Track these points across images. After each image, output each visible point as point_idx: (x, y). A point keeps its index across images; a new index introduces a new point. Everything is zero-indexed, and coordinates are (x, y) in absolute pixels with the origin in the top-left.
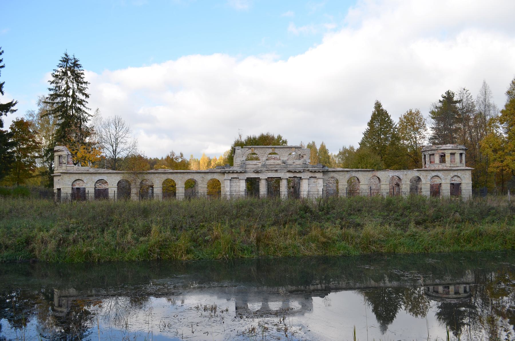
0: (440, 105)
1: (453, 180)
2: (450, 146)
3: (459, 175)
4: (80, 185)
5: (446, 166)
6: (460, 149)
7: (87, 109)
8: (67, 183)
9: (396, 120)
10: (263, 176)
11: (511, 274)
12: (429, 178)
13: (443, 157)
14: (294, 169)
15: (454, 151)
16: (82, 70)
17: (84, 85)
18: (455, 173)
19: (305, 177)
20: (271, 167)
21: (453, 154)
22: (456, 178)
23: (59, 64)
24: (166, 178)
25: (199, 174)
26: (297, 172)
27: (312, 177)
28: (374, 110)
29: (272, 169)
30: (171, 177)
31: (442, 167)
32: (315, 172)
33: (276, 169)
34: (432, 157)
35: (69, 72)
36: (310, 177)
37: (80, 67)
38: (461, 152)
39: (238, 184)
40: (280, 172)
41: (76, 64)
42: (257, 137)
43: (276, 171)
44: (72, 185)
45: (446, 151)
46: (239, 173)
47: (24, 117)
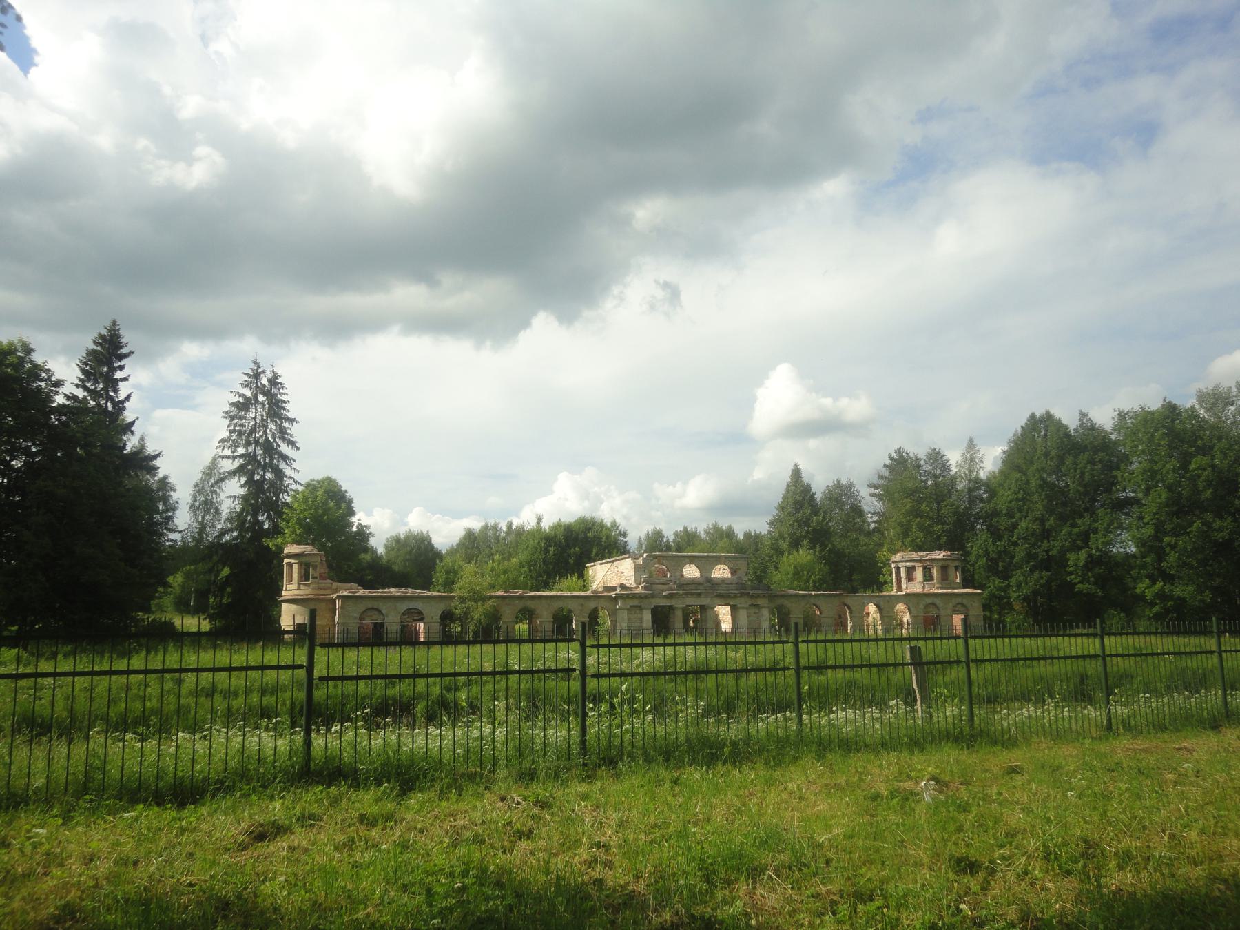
0: (886, 473)
3: (965, 601)
11: (790, 509)
15: (946, 563)
16: (284, 394)
17: (286, 425)
18: (959, 600)
19: (743, 605)
23: (245, 381)
35: (261, 398)
39: (639, 616)
41: (274, 382)
43: (699, 595)
44: (361, 618)
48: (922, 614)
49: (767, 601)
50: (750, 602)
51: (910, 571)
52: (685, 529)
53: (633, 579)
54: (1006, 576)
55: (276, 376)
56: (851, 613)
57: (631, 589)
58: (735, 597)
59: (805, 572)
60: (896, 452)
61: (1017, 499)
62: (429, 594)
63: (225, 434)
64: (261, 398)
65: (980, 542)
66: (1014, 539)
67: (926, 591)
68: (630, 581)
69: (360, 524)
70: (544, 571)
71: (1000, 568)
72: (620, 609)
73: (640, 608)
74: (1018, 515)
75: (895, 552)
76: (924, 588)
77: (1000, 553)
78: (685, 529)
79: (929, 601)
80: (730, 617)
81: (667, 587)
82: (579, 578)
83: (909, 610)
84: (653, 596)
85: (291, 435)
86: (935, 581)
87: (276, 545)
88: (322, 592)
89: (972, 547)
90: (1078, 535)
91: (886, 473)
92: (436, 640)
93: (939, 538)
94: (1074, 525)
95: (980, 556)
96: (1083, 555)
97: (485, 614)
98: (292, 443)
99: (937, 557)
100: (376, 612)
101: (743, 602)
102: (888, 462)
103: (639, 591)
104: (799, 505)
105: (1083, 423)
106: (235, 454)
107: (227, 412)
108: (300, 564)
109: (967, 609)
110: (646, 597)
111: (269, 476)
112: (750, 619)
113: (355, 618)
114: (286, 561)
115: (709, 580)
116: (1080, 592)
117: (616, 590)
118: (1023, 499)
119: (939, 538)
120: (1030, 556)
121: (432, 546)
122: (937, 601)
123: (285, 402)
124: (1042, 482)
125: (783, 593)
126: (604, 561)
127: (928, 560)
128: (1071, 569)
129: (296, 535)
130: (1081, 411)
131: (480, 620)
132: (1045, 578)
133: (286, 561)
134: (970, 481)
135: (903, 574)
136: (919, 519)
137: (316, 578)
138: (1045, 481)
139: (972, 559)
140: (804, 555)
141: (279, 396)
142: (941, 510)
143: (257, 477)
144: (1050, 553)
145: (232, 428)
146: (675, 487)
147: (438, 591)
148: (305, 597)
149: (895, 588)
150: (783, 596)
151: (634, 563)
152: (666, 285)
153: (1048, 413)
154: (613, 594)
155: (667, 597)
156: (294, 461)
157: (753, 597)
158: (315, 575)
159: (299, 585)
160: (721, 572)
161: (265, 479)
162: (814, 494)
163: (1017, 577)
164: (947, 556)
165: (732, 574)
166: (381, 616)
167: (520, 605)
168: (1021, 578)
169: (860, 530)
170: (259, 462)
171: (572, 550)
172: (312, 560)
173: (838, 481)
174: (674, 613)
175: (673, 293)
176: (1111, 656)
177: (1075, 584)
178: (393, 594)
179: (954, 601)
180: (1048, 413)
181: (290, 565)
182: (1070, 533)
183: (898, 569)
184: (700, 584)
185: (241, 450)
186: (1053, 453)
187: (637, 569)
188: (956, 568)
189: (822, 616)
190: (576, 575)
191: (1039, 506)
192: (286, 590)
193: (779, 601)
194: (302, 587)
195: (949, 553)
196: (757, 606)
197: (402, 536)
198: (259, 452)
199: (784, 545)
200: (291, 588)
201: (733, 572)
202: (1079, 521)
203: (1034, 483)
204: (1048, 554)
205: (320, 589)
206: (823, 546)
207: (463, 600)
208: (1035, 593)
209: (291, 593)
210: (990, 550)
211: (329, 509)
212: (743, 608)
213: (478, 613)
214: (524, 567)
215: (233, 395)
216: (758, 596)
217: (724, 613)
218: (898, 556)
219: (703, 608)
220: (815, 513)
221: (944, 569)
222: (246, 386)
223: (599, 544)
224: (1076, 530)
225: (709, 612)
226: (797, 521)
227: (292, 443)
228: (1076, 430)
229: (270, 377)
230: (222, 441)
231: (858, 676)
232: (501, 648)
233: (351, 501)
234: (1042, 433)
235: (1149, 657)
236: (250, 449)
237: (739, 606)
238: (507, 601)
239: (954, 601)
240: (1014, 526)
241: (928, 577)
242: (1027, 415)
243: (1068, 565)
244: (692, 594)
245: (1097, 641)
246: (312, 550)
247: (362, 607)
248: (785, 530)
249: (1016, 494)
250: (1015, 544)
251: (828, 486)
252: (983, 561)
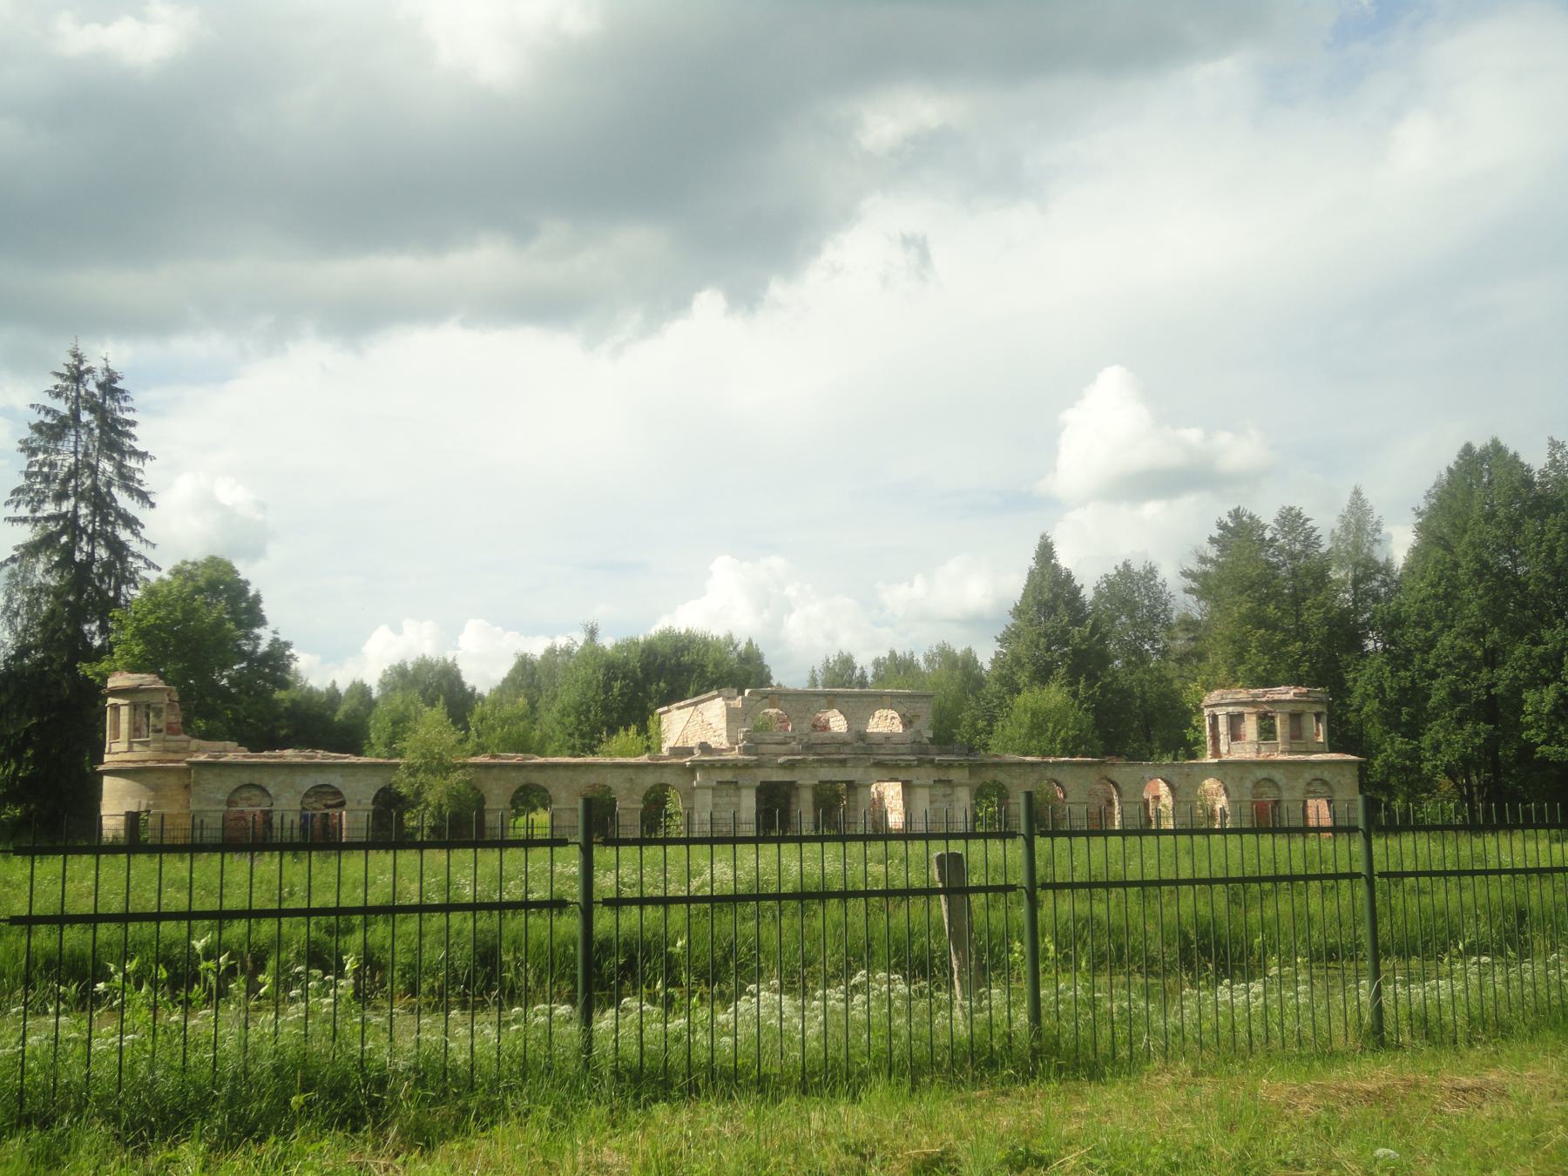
0: (1212, 552)
2: (1287, 693)
3: (1327, 776)
4: (254, 802)
7: (144, 545)
8: (212, 795)
10: (807, 779)
12: (1249, 784)
14: (893, 757)
15: (1300, 707)
16: (129, 409)
17: (131, 463)
18: (1317, 773)
20: (827, 749)
23: (56, 387)
25: (621, 770)
26: (903, 767)
27: (940, 781)
28: (1033, 564)
29: (831, 757)
33: (843, 756)
35: (86, 417)
36: (935, 781)
37: (125, 399)
38: (1319, 708)
39: (734, 799)
40: (853, 767)
41: (109, 387)
43: (843, 763)
46: (740, 768)
47: (271, 627)
48: (1250, 798)
49: (967, 772)
50: (935, 775)
51: (1235, 721)
52: (893, 654)
53: (725, 734)
54: (1413, 731)
55: (112, 377)
56: (1120, 795)
57: (720, 751)
58: (909, 766)
59: (1051, 725)
60: (1230, 516)
61: (1436, 596)
62: (363, 760)
63: (21, 481)
64: (86, 417)
65: (1368, 671)
66: (1430, 666)
67: (1261, 757)
68: (719, 739)
69: (276, 640)
70: (603, 723)
71: (1404, 718)
72: (700, 787)
74: (1437, 624)
75: (1209, 688)
76: (1258, 752)
77: (1403, 691)
78: (893, 654)
79: (1261, 774)
80: (901, 802)
81: (783, 748)
82: (639, 734)
83: (1226, 790)
84: (759, 765)
85: (140, 482)
86: (1279, 740)
87: (97, 674)
88: (171, 756)
89: (1355, 680)
90: (1544, 660)
91: (1212, 552)
92: (750, 835)
93: (1296, 665)
94: (1535, 642)
95: (1368, 695)
96: (1550, 694)
97: (450, 796)
98: (143, 497)
99: (1283, 697)
100: (257, 792)
101: (924, 776)
102: (1216, 533)
103: (735, 755)
104: (1048, 608)
105: (1555, 460)
106: (38, 514)
107: (25, 441)
108: (134, 707)
109: (1331, 789)
110: (746, 766)
111: (102, 553)
112: (936, 805)
113: (220, 802)
114: (111, 701)
115: (862, 737)
116: (1544, 761)
117: (693, 754)
118: (1446, 596)
119: (1296, 665)
120: (1456, 696)
121: (462, 684)
122: (1278, 775)
123: (133, 424)
124: (1477, 566)
125: (996, 759)
126: (682, 704)
127: (1267, 702)
128: (1530, 718)
129: (133, 656)
130: (1551, 439)
131: (440, 806)
132: (1483, 735)
133: (111, 701)
134: (1356, 565)
135: (1223, 728)
136: (1262, 631)
137: (160, 731)
138: (1485, 565)
139: (1355, 701)
140: (1054, 695)
141: (119, 414)
142: (1302, 615)
144: (1493, 692)
145: (36, 469)
146: (911, 585)
147: (378, 756)
148: (141, 765)
149: (1209, 752)
150: (996, 765)
151: (727, 705)
152: (907, 242)
153: (1495, 443)
154: (687, 761)
155: (783, 766)
156: (143, 527)
158: (159, 727)
159: (131, 743)
160: (884, 723)
161: (94, 560)
162: (1077, 591)
163: (1434, 732)
164: (1302, 695)
165: (905, 725)
166: (267, 799)
167: (519, 779)
168: (1440, 736)
170: (84, 530)
171: (654, 687)
172: (155, 699)
173: (1126, 565)
174: (798, 796)
175: (917, 246)
177: (1537, 745)
178: (288, 760)
179: (1308, 775)
180: (1495, 443)
181: (116, 708)
182: (1528, 655)
183: (1215, 718)
184: (845, 744)
185: (49, 508)
186: (1501, 513)
187: (732, 716)
188: (1318, 716)
189: (1067, 800)
190: (633, 729)
191: (1474, 607)
192: (109, 753)
193: (989, 776)
194: (136, 747)
195: (1304, 690)
196: (948, 783)
197: (410, 667)
198: (83, 510)
199: (1022, 678)
200: (117, 750)
201: (907, 723)
202: (1546, 634)
203: (1467, 565)
204: (1488, 693)
205: (166, 751)
206: (1092, 678)
207: (413, 771)
208: (1466, 761)
209: (117, 757)
210: (1386, 685)
211: (195, 610)
212: (922, 786)
213: (436, 791)
214: (569, 716)
215: (34, 411)
216: (950, 765)
217: (891, 793)
218: (1214, 696)
219: (851, 785)
220: (1078, 620)
221: (1295, 718)
222: (58, 395)
223: (702, 674)
224: (1540, 649)
225: (861, 793)
226: (1046, 635)
227: (143, 497)
228: (1544, 474)
229: (102, 379)
230: (17, 491)
231: (1099, 909)
232: (490, 858)
233: (257, 599)
234: (1485, 480)
235: (1344, 883)
236: (67, 506)
237: (915, 782)
238: (495, 772)
239: (1308, 775)
240: (1430, 644)
241: (1267, 732)
242: (1458, 447)
243: (1523, 712)
244: (830, 762)
245: (1358, 846)
246: (155, 682)
247: (231, 782)
248: (1021, 650)
249: (1433, 586)
250: (1432, 675)
251: (1106, 576)
252: (1372, 706)
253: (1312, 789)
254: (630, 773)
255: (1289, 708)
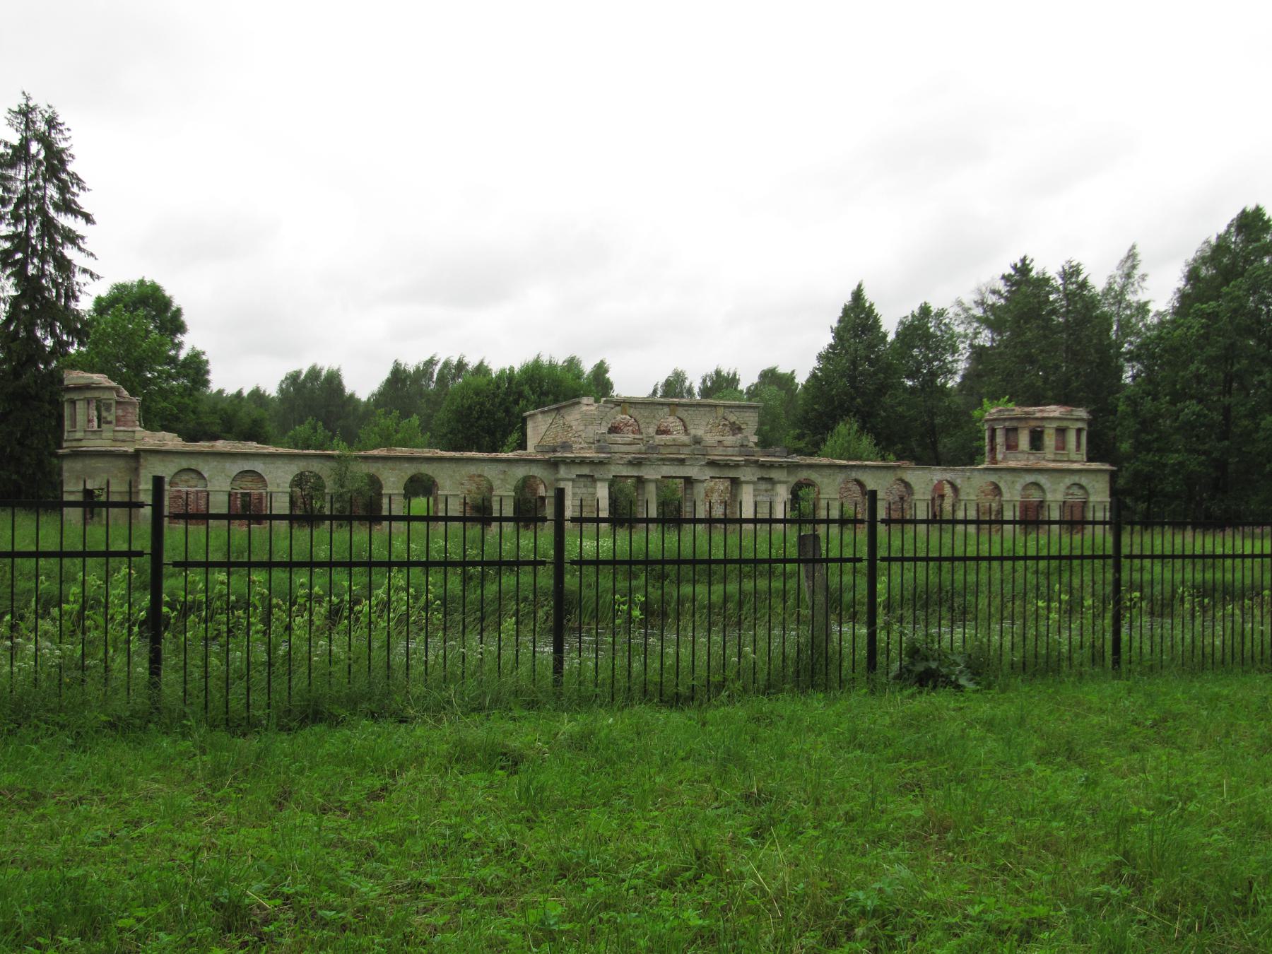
0: (1002, 287)
1: (1067, 494)
3: (1084, 481)
5: (1044, 459)
6: (1077, 420)
9: (890, 327)
13: (1036, 440)
15: (1064, 424)
18: (1076, 479)
19: (747, 479)
20: (669, 450)
21: (1061, 432)
22: (1075, 490)
24: (525, 474)
30: (426, 469)
31: (568, 418)
32: (124, 441)
34: (1011, 434)
35: (35, 147)
39: (590, 490)
41: (52, 123)
42: (560, 363)
45: (1046, 424)
46: (596, 464)
64: (35, 147)
73: (593, 479)
100: (194, 475)
126: (546, 409)
135: (1000, 439)
143: (31, 270)
157: (763, 466)
166: (202, 481)
169: (1149, 380)
176: (1131, 557)
179: (1068, 480)
196: (770, 480)
216: (771, 466)
237: (743, 479)
253: (1071, 491)
254: (502, 467)
255: (1055, 425)
